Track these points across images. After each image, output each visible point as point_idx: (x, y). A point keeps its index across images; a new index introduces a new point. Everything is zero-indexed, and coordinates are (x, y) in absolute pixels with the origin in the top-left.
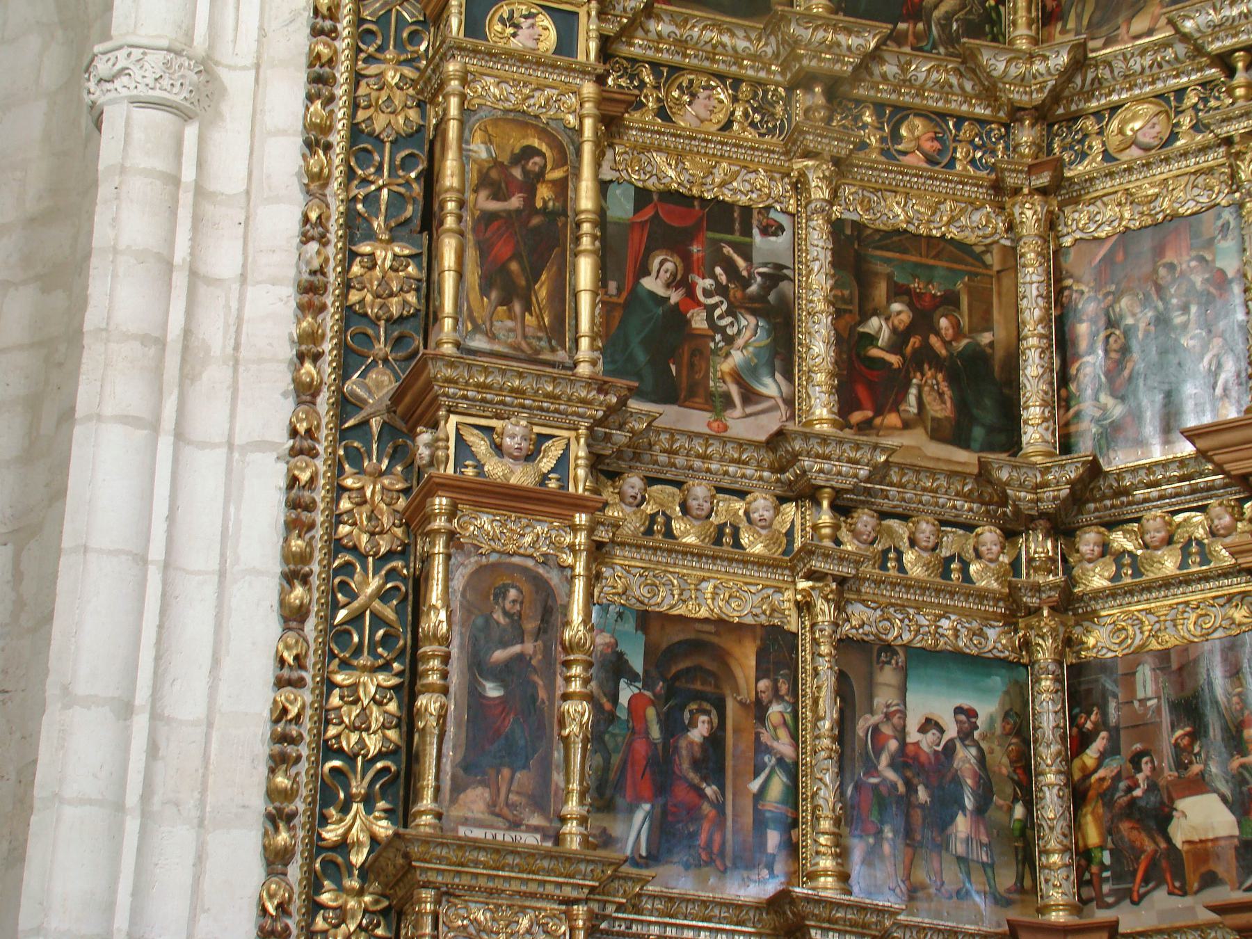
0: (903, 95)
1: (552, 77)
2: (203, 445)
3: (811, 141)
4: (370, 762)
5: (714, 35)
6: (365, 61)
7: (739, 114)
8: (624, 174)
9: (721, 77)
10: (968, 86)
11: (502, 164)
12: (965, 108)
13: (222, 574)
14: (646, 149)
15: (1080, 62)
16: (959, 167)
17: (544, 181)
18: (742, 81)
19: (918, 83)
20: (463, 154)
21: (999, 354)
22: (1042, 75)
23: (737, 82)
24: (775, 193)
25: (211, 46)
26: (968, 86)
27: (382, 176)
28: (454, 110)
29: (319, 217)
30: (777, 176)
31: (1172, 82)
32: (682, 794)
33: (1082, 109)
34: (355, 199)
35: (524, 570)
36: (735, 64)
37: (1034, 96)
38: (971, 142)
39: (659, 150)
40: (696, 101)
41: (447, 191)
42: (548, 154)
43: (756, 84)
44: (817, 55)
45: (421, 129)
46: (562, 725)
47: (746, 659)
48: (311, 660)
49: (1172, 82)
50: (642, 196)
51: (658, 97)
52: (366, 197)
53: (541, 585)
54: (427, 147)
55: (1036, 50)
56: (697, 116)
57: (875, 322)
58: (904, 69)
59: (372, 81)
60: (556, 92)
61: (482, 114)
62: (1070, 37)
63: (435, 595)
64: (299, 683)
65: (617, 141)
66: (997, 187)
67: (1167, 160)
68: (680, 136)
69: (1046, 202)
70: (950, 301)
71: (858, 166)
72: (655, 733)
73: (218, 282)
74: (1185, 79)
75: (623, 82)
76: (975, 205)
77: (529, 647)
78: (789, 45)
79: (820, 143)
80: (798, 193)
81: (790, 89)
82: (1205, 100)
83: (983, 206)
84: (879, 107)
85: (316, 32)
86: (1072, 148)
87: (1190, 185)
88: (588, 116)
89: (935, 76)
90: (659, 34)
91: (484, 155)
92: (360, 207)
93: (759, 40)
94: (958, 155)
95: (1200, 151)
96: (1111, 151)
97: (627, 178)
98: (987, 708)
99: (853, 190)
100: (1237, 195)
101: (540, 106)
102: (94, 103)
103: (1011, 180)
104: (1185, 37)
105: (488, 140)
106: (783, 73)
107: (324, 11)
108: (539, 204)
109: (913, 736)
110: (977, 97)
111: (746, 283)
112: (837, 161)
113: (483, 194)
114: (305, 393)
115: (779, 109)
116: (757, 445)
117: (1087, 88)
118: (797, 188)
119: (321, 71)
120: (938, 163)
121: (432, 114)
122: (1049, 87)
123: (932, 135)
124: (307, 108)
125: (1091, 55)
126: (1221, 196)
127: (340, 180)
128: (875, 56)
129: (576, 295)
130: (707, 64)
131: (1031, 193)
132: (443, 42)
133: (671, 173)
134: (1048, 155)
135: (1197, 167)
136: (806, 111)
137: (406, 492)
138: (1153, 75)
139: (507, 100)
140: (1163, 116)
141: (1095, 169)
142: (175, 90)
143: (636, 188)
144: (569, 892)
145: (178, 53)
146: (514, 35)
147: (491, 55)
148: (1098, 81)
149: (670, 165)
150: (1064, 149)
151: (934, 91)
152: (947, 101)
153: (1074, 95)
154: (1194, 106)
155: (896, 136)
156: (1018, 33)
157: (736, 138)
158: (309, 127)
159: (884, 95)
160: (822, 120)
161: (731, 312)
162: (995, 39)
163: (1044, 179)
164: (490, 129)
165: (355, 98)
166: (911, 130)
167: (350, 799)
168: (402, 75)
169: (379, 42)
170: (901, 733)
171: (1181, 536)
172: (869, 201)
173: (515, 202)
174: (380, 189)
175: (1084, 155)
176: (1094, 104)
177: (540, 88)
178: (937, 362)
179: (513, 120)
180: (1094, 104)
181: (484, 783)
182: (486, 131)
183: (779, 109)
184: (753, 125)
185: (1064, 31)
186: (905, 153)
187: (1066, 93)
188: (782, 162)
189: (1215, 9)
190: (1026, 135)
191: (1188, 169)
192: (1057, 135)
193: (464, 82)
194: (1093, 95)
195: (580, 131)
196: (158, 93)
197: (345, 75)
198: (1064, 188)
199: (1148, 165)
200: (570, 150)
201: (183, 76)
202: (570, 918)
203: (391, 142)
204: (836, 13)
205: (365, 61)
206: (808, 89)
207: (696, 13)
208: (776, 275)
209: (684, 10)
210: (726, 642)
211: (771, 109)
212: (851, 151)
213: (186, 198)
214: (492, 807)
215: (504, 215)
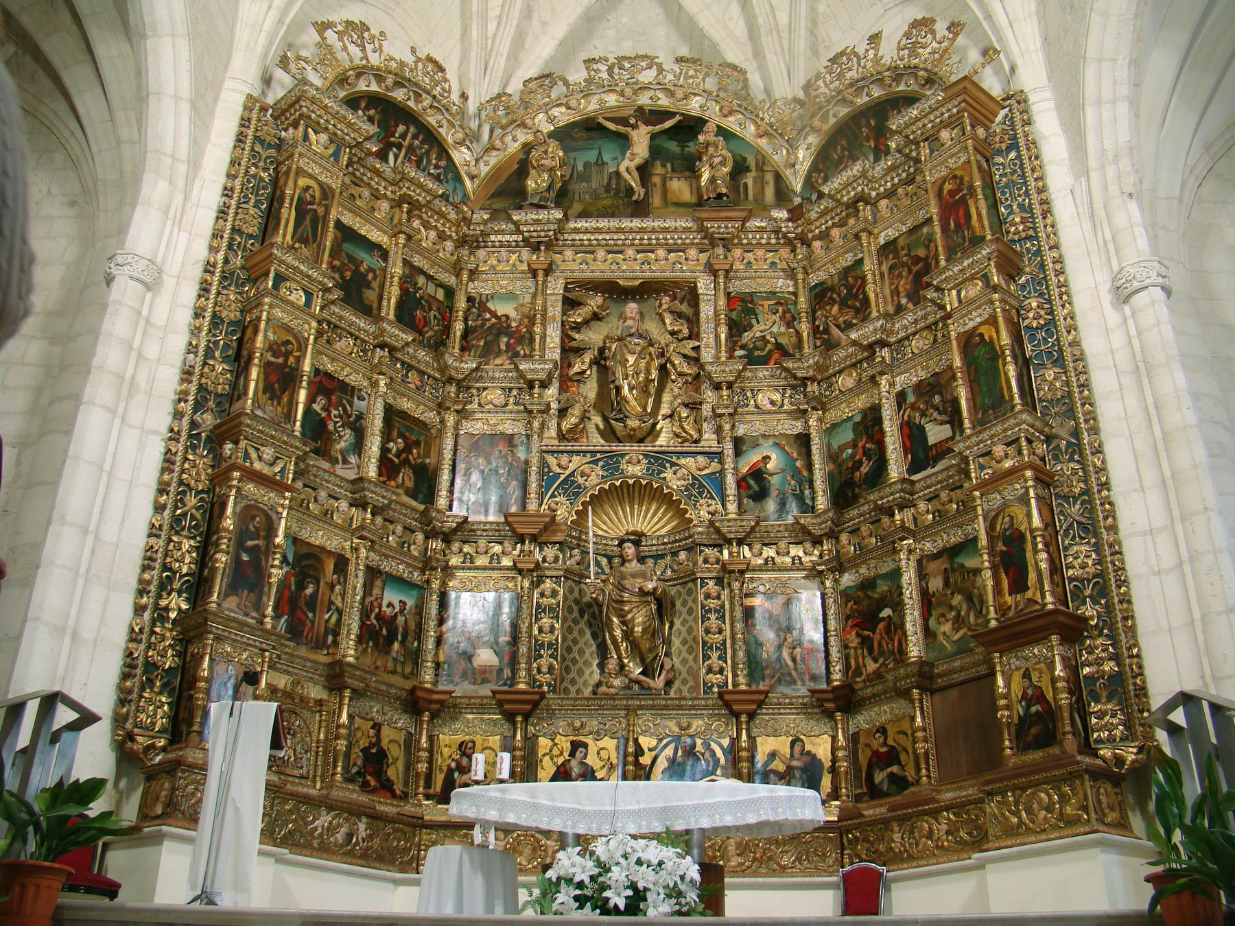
2: (131, 427)
3: (384, 369)
4: (182, 577)
9: (352, 335)
13: (131, 482)
14: (321, 353)
20: (265, 337)
21: (431, 467)
32: (299, 614)
35: (263, 510)
43: (363, 341)
46: (270, 577)
47: (330, 565)
48: (165, 528)
53: (268, 517)
57: (392, 444)
58: (416, 351)
63: (229, 511)
64: (159, 537)
66: (440, 405)
70: (417, 443)
72: (293, 588)
73: (147, 360)
76: (431, 410)
77: (261, 542)
81: (375, 347)
85: (206, 271)
98: (410, 603)
105: (274, 333)
109: (384, 608)
111: (350, 416)
114: (178, 415)
116: (348, 481)
129: (297, 403)
137: (212, 466)
144: (264, 646)
147: (282, 300)
148: (482, 377)
161: (342, 426)
163: (459, 407)
167: (172, 590)
170: (380, 606)
171: (491, 552)
173: (281, 360)
178: (411, 466)
181: (237, 595)
195: (308, 340)
202: (263, 657)
208: (360, 417)
210: (324, 557)
213: (142, 322)
214: (238, 606)
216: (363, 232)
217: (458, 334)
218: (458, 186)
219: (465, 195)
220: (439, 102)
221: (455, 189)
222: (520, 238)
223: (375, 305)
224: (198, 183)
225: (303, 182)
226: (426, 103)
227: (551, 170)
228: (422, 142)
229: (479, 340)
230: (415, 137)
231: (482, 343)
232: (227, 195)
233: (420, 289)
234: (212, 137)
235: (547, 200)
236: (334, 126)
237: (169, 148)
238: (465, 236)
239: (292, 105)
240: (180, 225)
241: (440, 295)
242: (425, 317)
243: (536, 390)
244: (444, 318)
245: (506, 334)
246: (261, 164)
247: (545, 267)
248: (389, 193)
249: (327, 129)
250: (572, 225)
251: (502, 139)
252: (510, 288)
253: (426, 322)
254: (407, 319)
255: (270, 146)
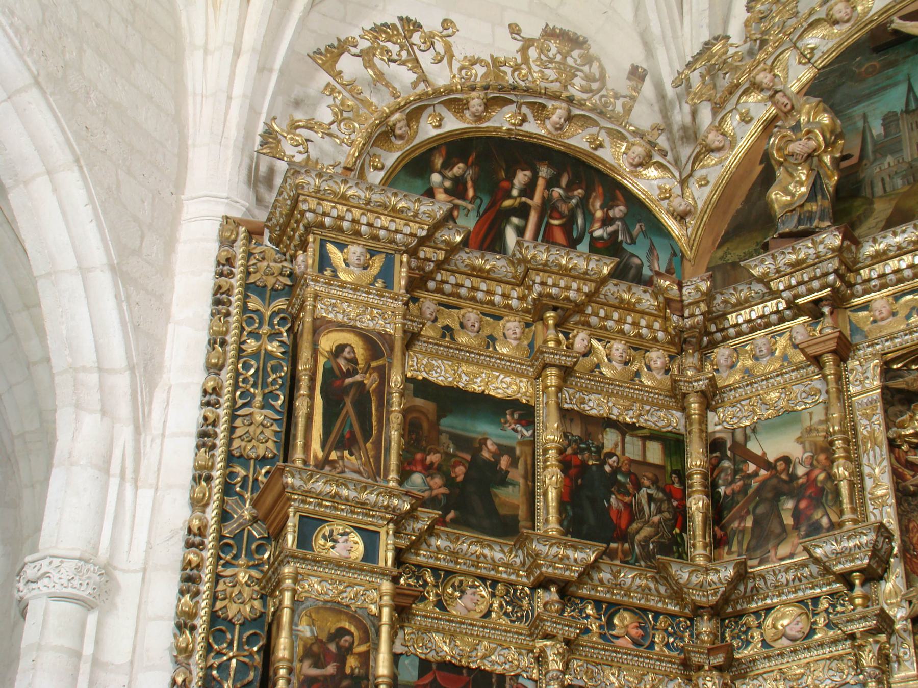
0: (615, 594)
1: (360, 578)
3: (548, 627)
5: (477, 549)
6: (224, 565)
7: (496, 605)
8: (411, 649)
9: (483, 579)
10: (662, 589)
11: (321, 641)
12: (660, 605)
14: (428, 630)
15: (742, 575)
16: (657, 648)
17: (352, 654)
18: (498, 582)
19: (625, 587)
22: (715, 583)
23: (494, 583)
24: (522, 664)
25: (111, 556)
26: (662, 589)
27: (232, 650)
28: (287, 601)
29: (184, 681)
30: (524, 652)
31: (809, 592)
33: (745, 609)
34: (211, 667)
36: (493, 569)
37: (710, 598)
38: (666, 630)
39: (437, 631)
40: (465, 596)
41: (280, 661)
42: (356, 634)
43: (509, 584)
44: (552, 564)
45: (262, 615)
49: (809, 592)
50: (425, 666)
51: (437, 593)
52: (220, 665)
54: (266, 628)
55: (710, 565)
56: (465, 607)
58: (615, 575)
59: (228, 580)
60: (362, 588)
61: (308, 604)
62: (735, 556)
65: (406, 624)
66: (686, 664)
67: (808, 649)
68: (452, 621)
69: (722, 677)
71: (583, 646)
74: (818, 590)
75: (411, 581)
78: (532, 557)
79: (555, 628)
80: (539, 665)
81: (533, 588)
82: (834, 606)
83: (675, 678)
84: (598, 603)
85: (189, 545)
86: (739, 637)
87: (826, 668)
88: (386, 606)
89: (638, 581)
90: (438, 548)
91: (308, 634)
92: (215, 673)
93: (511, 553)
94: (656, 640)
95: (832, 642)
96: (767, 640)
97: (413, 651)
99: (580, 663)
100: (861, 677)
101: (351, 599)
102: (22, 598)
103: (696, 659)
104: (817, 561)
105: (312, 623)
106: (528, 577)
107: (195, 530)
108: (348, 671)
110: (669, 598)
112: (568, 642)
113: (307, 663)
115: (525, 603)
117: (748, 593)
118: (538, 661)
119: (191, 573)
120: (641, 645)
121: (271, 604)
122: (720, 592)
123: (637, 624)
124: (179, 600)
125: (750, 570)
126: (850, 677)
127: (200, 653)
128: (594, 566)
130: (472, 569)
131: (710, 670)
132: (281, 552)
133: (446, 649)
134: (722, 642)
135: (831, 655)
136: (545, 605)
138: (795, 587)
139: (326, 594)
140: (804, 617)
141: (757, 653)
142: (82, 588)
143: (420, 659)
145: (87, 561)
146: (333, 547)
147: (315, 561)
148: (755, 589)
149: (445, 642)
150: (733, 638)
151: (638, 593)
152: (647, 600)
153: (738, 599)
154: (826, 610)
155: (610, 625)
156: (697, 552)
157: (494, 623)
158: (180, 613)
159: (602, 594)
160: (557, 611)
162: (680, 557)
163: (719, 660)
164: (313, 615)
165: (215, 592)
166: (622, 620)
168: (250, 576)
169: (234, 552)
172: (592, 672)
173: (330, 669)
174: (230, 659)
175: (748, 643)
176: (754, 605)
177: (350, 585)
179: (330, 609)
180: (754, 605)
182: (310, 616)
183: (525, 603)
184: (506, 614)
185: (730, 553)
186: (617, 637)
187: (733, 597)
188: (528, 641)
189: (837, 542)
190: (705, 627)
191: (824, 656)
192: (728, 627)
193: (296, 580)
194: (753, 600)
195: (379, 617)
196: (70, 590)
197: (208, 576)
198: (735, 666)
199: (795, 652)
200: (372, 631)
201: (89, 578)
203: (240, 625)
204: (566, 535)
205: (224, 565)
206: (546, 588)
207: (465, 533)
209: (456, 531)
211: (519, 603)
212: (578, 635)
215: (322, 679)
216: (477, 387)
217: (698, 518)
218: (657, 241)
219: (676, 254)
220: (581, 105)
221: (652, 249)
222: (782, 306)
223: (522, 512)
224: (159, 396)
225: (327, 342)
226: (558, 116)
227: (810, 157)
228: (569, 188)
229: (743, 519)
230: (552, 183)
231: (749, 523)
232: (208, 404)
233: (610, 455)
234: (175, 309)
235: (811, 217)
236: (370, 225)
237: (88, 357)
238: (680, 331)
239: (291, 214)
240: (136, 480)
241: (655, 453)
242: (628, 506)
243: (858, 591)
244: (669, 496)
245: (791, 495)
246: (265, 329)
247: (832, 345)
248: (514, 303)
249: (358, 234)
250: (869, 249)
251: (718, 128)
252: (782, 403)
253: (634, 514)
254: (591, 519)
255: (276, 293)
